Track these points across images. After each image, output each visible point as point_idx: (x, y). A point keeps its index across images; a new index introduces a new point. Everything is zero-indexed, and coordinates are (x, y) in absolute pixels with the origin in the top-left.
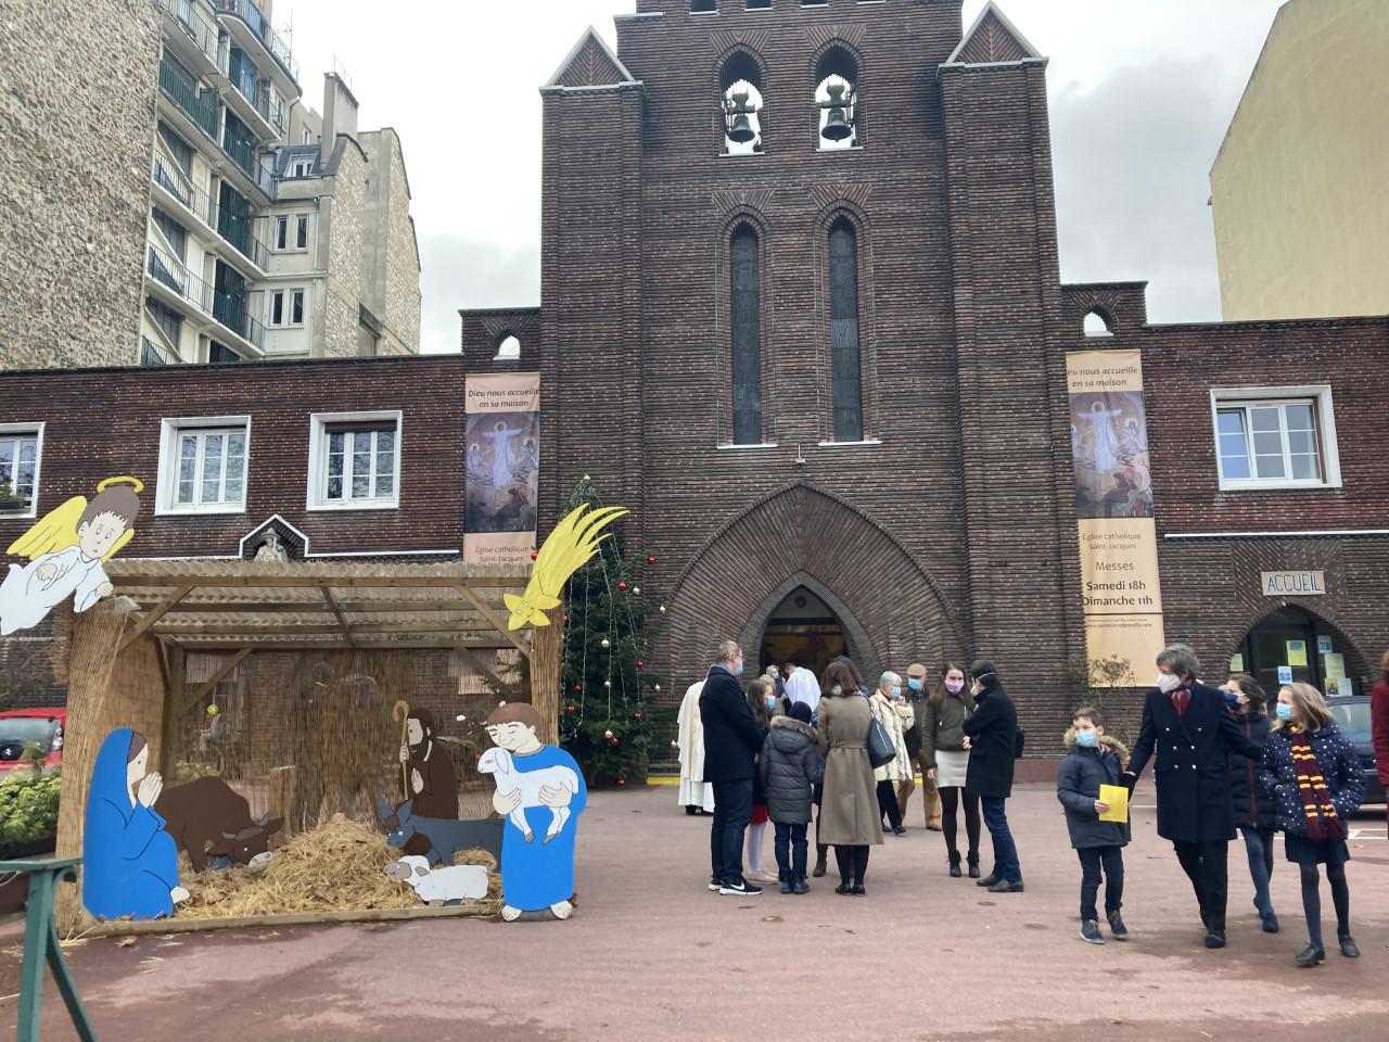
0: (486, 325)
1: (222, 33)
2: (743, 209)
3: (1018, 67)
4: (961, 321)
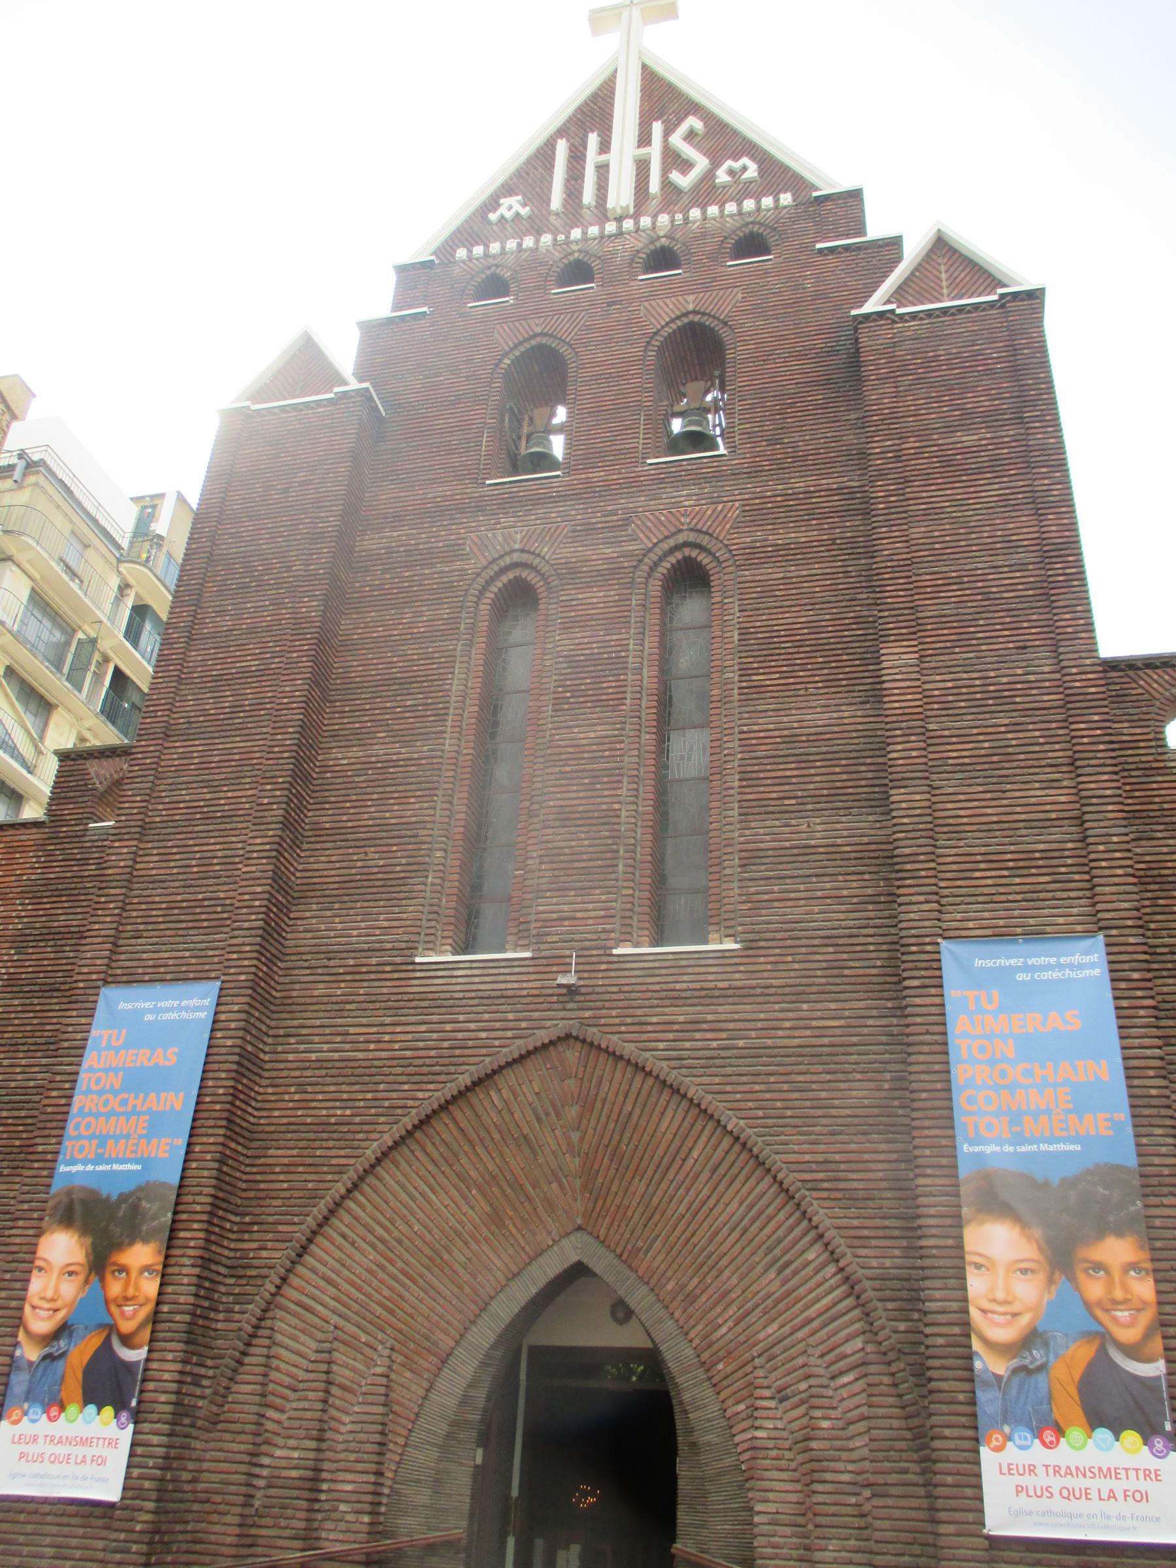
0: (92, 771)
1: (124, 587)
2: (516, 557)
3: (991, 305)
4: (894, 703)
